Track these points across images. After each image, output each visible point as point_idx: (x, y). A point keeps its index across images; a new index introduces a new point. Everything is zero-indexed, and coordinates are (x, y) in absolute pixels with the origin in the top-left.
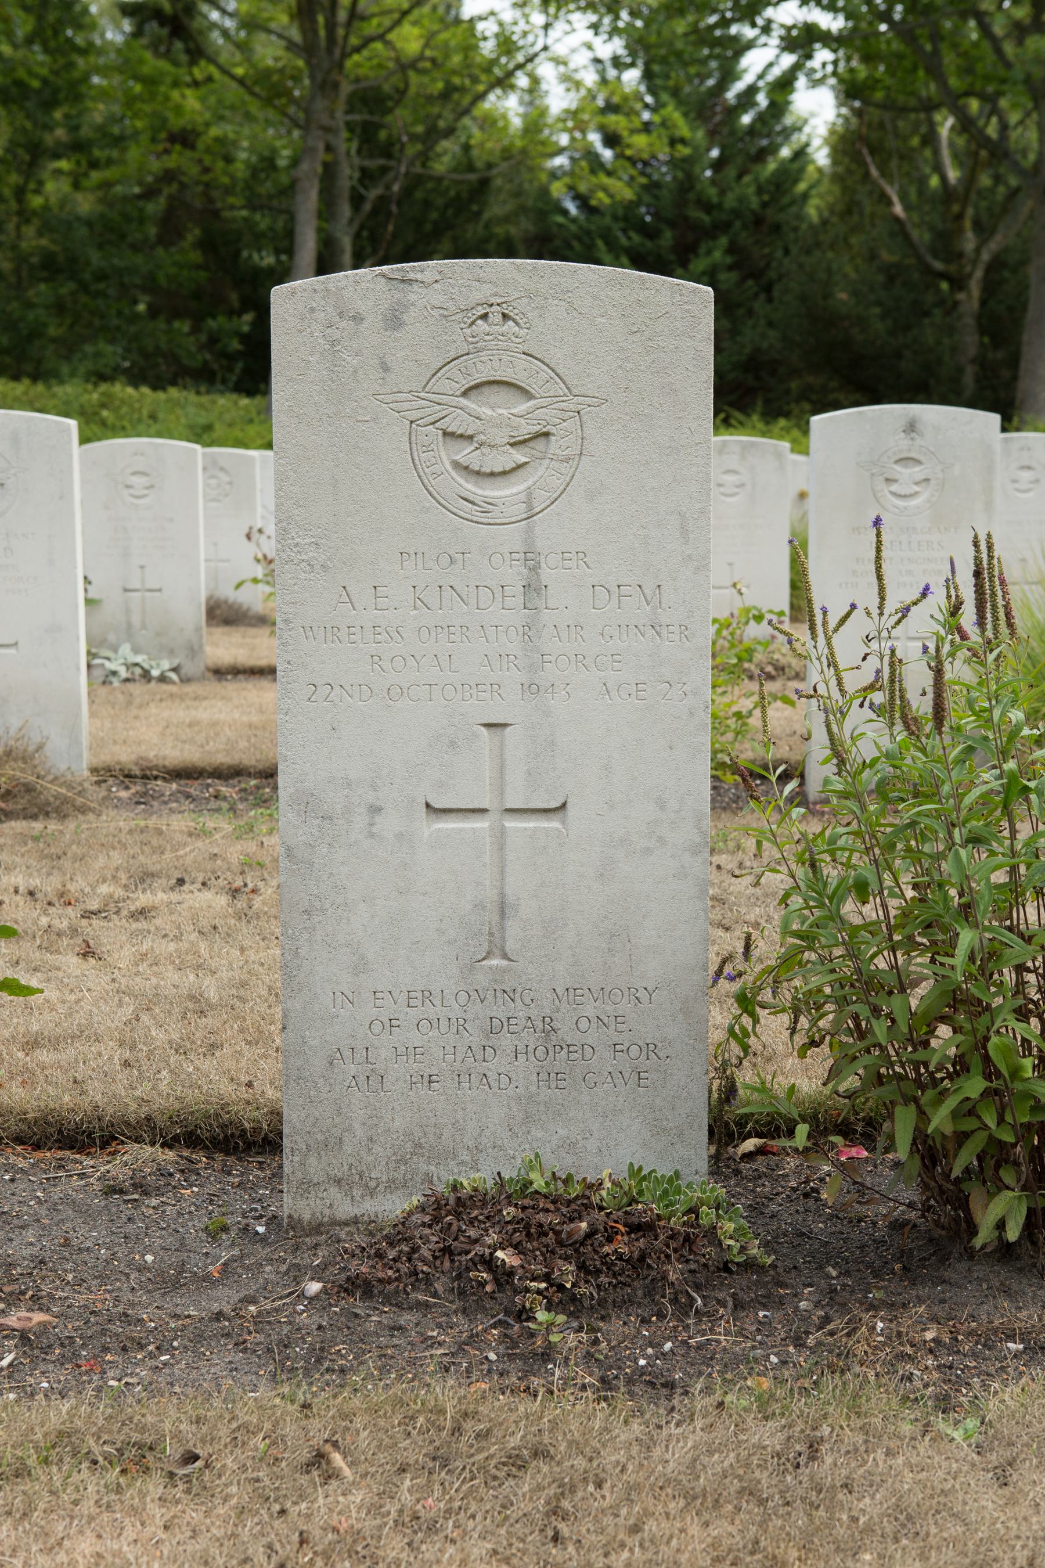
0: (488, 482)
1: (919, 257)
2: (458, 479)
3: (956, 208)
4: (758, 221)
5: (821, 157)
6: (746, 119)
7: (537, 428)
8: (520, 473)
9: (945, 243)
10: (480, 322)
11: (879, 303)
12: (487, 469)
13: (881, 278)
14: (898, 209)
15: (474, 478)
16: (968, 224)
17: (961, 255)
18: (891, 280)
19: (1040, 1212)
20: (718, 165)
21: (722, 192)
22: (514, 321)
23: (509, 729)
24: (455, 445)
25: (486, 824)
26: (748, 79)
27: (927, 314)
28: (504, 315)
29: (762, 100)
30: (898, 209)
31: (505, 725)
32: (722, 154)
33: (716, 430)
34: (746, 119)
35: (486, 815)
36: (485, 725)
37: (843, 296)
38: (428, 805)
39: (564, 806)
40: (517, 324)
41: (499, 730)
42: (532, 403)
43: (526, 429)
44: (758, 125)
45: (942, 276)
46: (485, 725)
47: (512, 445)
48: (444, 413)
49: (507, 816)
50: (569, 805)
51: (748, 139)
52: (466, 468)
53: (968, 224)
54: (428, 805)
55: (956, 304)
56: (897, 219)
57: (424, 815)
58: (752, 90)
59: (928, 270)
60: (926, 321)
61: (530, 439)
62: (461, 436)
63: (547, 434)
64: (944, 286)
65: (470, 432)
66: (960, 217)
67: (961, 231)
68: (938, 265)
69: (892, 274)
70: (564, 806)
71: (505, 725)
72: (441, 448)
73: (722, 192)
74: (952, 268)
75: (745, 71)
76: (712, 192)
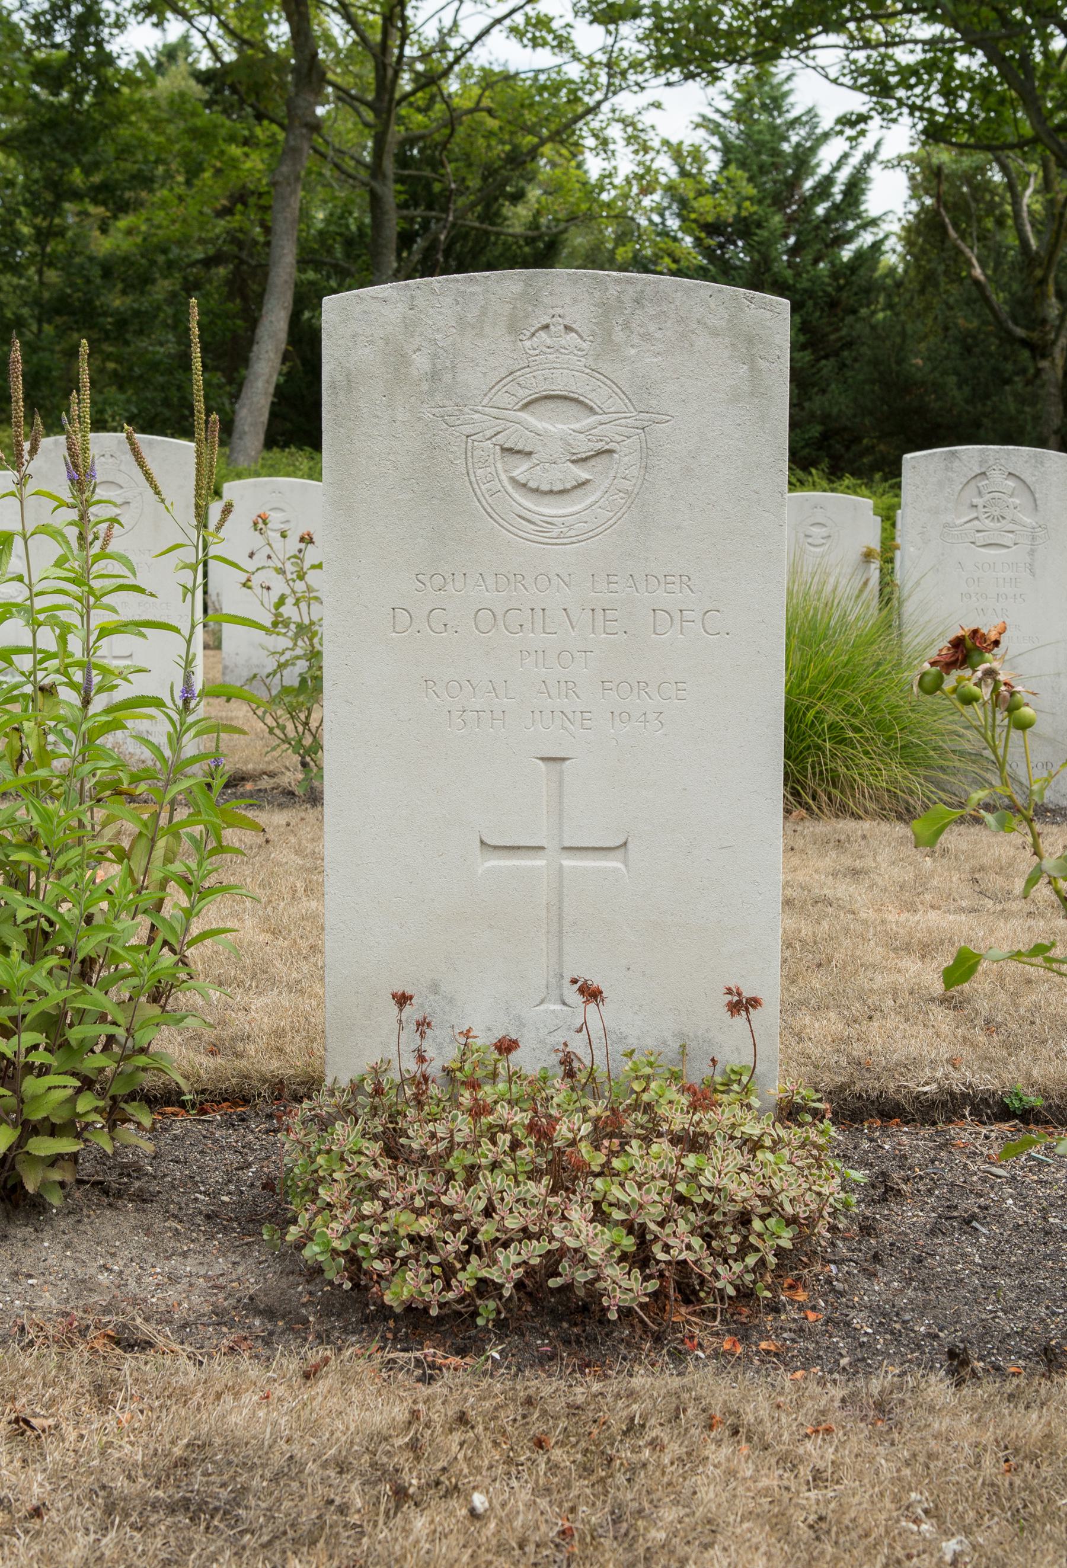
0: (547, 499)
1: (999, 323)
2: (516, 496)
3: (1039, 273)
4: (833, 304)
5: (893, 257)
6: (820, 210)
7: (599, 446)
8: (580, 492)
9: (1027, 308)
10: (542, 333)
11: (957, 373)
12: (545, 487)
13: (956, 349)
14: (977, 272)
15: (535, 496)
16: (1051, 289)
17: (1044, 322)
18: (968, 350)
19: (18, 407)
20: (793, 251)
21: (798, 275)
22: (576, 332)
23: (568, 762)
24: (511, 459)
25: (544, 862)
26: (824, 170)
27: (1008, 381)
28: (566, 327)
29: (837, 190)
30: (977, 272)
31: (564, 759)
32: (796, 243)
33: (792, 486)
34: (820, 210)
35: (541, 853)
36: (542, 759)
37: (919, 362)
38: (482, 842)
39: (625, 844)
40: (581, 337)
41: (557, 766)
42: (594, 419)
43: (584, 447)
44: (833, 213)
45: (1025, 343)
46: (542, 759)
47: (573, 462)
48: (498, 429)
49: (565, 854)
50: (630, 846)
51: (824, 226)
52: (524, 485)
53: (1051, 289)
54: (482, 842)
55: (1039, 371)
56: (976, 282)
57: (478, 852)
58: (828, 181)
59: (1009, 338)
60: (1007, 388)
61: (592, 456)
62: (519, 452)
63: (610, 452)
64: (1026, 354)
65: (527, 449)
66: (1042, 282)
67: (1044, 296)
68: (1020, 332)
69: (968, 344)
70: (625, 844)
71: (564, 759)
72: (499, 465)
73: (798, 275)
74: (1035, 335)
75: (818, 165)
76: (789, 273)
